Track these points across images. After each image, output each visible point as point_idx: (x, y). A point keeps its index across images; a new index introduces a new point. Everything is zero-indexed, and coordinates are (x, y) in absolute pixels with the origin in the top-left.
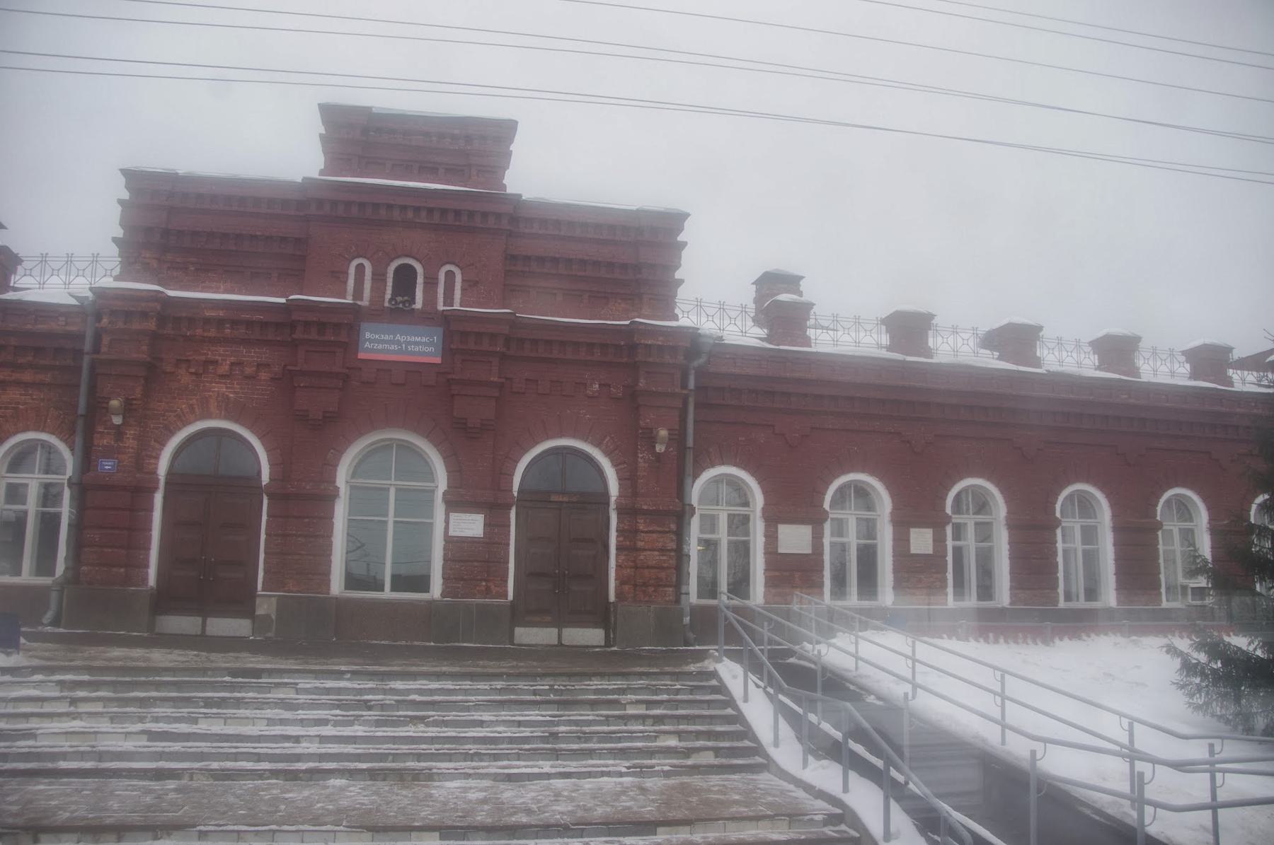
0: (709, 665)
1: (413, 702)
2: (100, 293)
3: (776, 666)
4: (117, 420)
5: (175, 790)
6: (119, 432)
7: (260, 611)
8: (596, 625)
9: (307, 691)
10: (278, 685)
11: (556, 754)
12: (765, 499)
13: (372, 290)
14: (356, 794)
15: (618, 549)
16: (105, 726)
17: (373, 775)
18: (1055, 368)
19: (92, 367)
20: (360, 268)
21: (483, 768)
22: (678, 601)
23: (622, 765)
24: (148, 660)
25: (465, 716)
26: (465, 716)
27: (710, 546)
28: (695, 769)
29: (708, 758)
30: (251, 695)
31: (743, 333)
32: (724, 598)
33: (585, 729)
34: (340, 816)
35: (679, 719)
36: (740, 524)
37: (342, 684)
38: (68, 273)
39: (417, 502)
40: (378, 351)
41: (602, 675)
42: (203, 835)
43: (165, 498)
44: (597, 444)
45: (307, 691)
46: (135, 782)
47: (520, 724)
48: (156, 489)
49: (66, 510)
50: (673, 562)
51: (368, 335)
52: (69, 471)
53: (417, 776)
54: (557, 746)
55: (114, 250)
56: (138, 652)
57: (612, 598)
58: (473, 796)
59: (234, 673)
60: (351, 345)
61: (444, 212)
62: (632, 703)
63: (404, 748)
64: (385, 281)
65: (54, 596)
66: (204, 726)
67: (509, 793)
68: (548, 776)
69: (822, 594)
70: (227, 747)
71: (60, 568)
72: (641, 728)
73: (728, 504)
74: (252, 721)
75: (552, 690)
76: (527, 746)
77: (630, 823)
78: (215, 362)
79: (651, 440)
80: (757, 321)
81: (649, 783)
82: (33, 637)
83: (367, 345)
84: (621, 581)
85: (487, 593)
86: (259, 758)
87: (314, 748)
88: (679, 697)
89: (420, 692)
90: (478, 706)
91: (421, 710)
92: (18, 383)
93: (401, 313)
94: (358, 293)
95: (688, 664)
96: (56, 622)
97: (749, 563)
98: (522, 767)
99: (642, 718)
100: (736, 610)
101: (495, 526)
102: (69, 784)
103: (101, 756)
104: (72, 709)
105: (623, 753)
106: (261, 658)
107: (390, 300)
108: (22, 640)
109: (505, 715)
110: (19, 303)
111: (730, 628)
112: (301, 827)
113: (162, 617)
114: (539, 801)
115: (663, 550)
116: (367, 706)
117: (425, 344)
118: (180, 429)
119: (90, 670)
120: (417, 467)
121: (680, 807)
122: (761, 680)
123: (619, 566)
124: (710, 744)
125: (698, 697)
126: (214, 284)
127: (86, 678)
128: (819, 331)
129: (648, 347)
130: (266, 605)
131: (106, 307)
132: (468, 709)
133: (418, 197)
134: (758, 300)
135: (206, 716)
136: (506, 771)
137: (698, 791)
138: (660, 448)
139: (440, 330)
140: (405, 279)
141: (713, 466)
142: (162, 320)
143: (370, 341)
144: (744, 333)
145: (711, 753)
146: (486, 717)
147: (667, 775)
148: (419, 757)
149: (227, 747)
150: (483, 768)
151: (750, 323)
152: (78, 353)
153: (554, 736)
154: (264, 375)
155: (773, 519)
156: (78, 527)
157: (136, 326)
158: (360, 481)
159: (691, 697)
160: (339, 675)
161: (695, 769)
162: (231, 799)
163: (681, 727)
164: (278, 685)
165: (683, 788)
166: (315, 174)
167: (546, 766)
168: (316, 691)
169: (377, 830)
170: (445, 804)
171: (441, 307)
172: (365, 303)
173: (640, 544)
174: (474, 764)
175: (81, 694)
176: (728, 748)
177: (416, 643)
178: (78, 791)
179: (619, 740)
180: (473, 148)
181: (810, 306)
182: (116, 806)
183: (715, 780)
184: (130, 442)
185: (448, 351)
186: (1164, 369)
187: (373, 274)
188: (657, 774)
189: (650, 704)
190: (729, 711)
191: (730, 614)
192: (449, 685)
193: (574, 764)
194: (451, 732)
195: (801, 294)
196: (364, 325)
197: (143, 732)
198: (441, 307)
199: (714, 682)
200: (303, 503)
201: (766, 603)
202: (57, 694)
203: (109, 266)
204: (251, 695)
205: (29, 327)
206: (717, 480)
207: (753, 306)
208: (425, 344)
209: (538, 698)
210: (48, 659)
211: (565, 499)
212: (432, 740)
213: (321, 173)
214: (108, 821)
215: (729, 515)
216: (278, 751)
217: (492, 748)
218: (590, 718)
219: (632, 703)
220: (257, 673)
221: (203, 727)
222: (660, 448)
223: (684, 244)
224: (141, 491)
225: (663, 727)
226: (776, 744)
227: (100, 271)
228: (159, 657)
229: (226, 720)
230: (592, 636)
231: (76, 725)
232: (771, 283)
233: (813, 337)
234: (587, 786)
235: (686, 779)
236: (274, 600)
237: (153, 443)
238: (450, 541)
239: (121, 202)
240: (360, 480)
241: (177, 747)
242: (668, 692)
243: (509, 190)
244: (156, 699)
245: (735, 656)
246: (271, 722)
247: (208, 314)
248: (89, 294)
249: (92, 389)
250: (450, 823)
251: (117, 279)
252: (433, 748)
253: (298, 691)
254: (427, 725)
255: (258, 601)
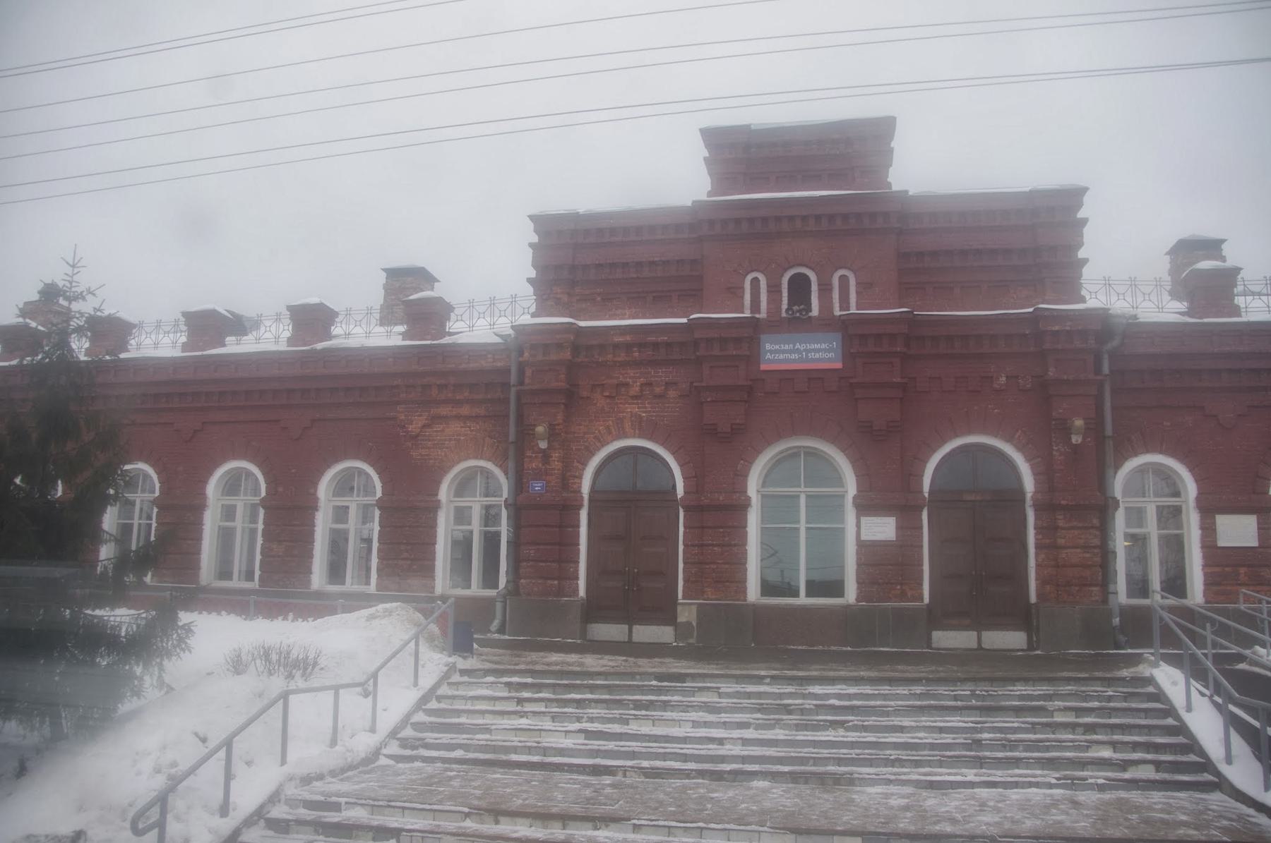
0: (1144, 670)
1: (833, 707)
2: (519, 329)
3: (1225, 673)
4: (543, 445)
5: (611, 785)
6: (546, 456)
7: (682, 618)
8: (1016, 628)
9: (728, 695)
10: (701, 689)
11: (980, 762)
12: (1199, 489)
13: (768, 303)
14: (779, 796)
15: (1038, 547)
16: (548, 724)
17: (794, 778)
18: (353, 343)
19: (518, 398)
20: (843, 279)
21: (905, 774)
22: (1105, 601)
23: (1052, 776)
24: (581, 664)
25: (884, 721)
26: (884, 721)
27: (1138, 542)
28: (1134, 784)
29: (1147, 773)
30: (676, 698)
31: (1165, 310)
32: (1158, 597)
33: (1009, 736)
34: (763, 817)
35: (1113, 728)
36: (1171, 515)
37: (762, 688)
38: (492, 315)
39: (827, 507)
40: (780, 361)
41: (1026, 680)
42: (637, 828)
43: (589, 514)
44: (1009, 439)
45: (728, 695)
46: (575, 776)
47: (941, 730)
48: (581, 506)
49: (504, 529)
50: (1098, 559)
51: (768, 346)
52: (505, 495)
53: (838, 780)
54: (980, 754)
55: (530, 290)
56: (573, 658)
57: (1033, 598)
58: (894, 802)
59: (660, 677)
60: (753, 358)
61: (831, 218)
62: (1060, 710)
63: (825, 753)
64: (780, 292)
65: (499, 606)
66: (635, 728)
67: (931, 801)
68: (972, 785)
69: (429, 571)
70: (655, 747)
71: (502, 581)
72: (1071, 736)
73: (1156, 495)
74: (678, 722)
75: (973, 695)
76: (948, 753)
77: (1062, 838)
78: (627, 385)
79: (1066, 431)
80: (1174, 295)
81: (1082, 796)
82: (483, 643)
83: (768, 356)
84: (1042, 582)
85: (903, 596)
86: (685, 758)
87: (737, 750)
88: (1112, 704)
89: (839, 696)
90: (897, 712)
91: (841, 714)
92: (458, 417)
93: (798, 322)
94: (755, 306)
95: (1120, 669)
96: (501, 630)
97: (1183, 558)
98: (944, 775)
99: (1072, 727)
100: (1171, 609)
101: (908, 528)
102: (520, 774)
103: (545, 751)
104: (519, 708)
105: (1051, 764)
106: (684, 663)
107: (787, 310)
108: (475, 646)
109: (926, 721)
110: (454, 345)
111: (1166, 630)
112: (727, 826)
113: (594, 625)
114: (964, 811)
115: (1086, 548)
116: (788, 710)
117: (825, 350)
118: (599, 449)
119: (532, 673)
120: (823, 473)
121: (1118, 824)
122: (1207, 687)
123: (1038, 565)
124: (1149, 757)
125: (1134, 705)
126: (619, 312)
127: (529, 680)
128: (1249, 298)
129: (1056, 334)
130: (687, 613)
131: (526, 339)
132: (887, 714)
133: (801, 203)
134: (1175, 271)
135: (636, 718)
136: (929, 778)
137: (1137, 808)
138: (1076, 439)
139: (839, 336)
140: (800, 288)
141: (1136, 455)
142: (576, 349)
143: (771, 352)
144: (1160, 309)
145: (1151, 767)
146: (907, 722)
147: (1101, 788)
148: (840, 761)
149: (655, 747)
150: (905, 774)
151: (1166, 297)
152: (506, 386)
153: (978, 743)
154: (672, 394)
155: (1209, 509)
156: (515, 544)
157: (553, 357)
158: (771, 490)
159: (1125, 705)
160: (759, 680)
161: (1134, 784)
162: (662, 796)
163: (1115, 737)
164: (701, 689)
165: (1121, 804)
166: (703, 197)
167: (970, 775)
168: (738, 695)
169: (797, 831)
170: (866, 809)
171: (837, 312)
172: (763, 315)
173: (1061, 542)
174: (895, 770)
175: (526, 695)
176: (1170, 762)
177: (833, 648)
178: (528, 782)
179: (1047, 749)
180: (846, 151)
181: (1237, 270)
182: (560, 797)
183: (1157, 797)
184: (556, 465)
185: (848, 356)
186: (166, 340)
187: (768, 286)
188: (1091, 787)
189: (1079, 711)
190: (1170, 721)
191: (1166, 615)
192: (868, 690)
193: (999, 773)
194: (871, 738)
195: (1223, 259)
196: (763, 337)
197: (580, 731)
198: (837, 312)
199: (1151, 689)
200: (718, 515)
201: (1207, 602)
202: (506, 694)
203: (526, 304)
204: (676, 698)
205: (463, 366)
206: (1142, 470)
207: (1169, 278)
208: (825, 350)
209: (959, 703)
210: (496, 663)
211: (978, 498)
212: (852, 745)
213: (710, 194)
214: (554, 810)
215: (1158, 507)
216: (702, 752)
217: (912, 755)
218: (1016, 725)
219: (1060, 710)
220: (681, 678)
221: (633, 728)
222: (1076, 439)
223: (1084, 222)
224: (568, 508)
225: (1095, 737)
226: (1229, 760)
227: (519, 311)
228: (591, 662)
229: (654, 721)
230: (1013, 639)
231: (524, 722)
232: (1189, 249)
233: (1242, 306)
234: (1014, 797)
235: (1123, 794)
236: (694, 608)
237: (576, 464)
238: (862, 546)
239: (531, 245)
240: (771, 489)
241: (611, 745)
242: (1099, 698)
243: (895, 188)
244: (590, 701)
245: (1175, 661)
246: (696, 724)
247: (618, 339)
248: (511, 332)
249: (520, 417)
250: (872, 829)
251: (533, 315)
252: (853, 753)
253: (720, 695)
254: (847, 729)
255: (679, 608)
